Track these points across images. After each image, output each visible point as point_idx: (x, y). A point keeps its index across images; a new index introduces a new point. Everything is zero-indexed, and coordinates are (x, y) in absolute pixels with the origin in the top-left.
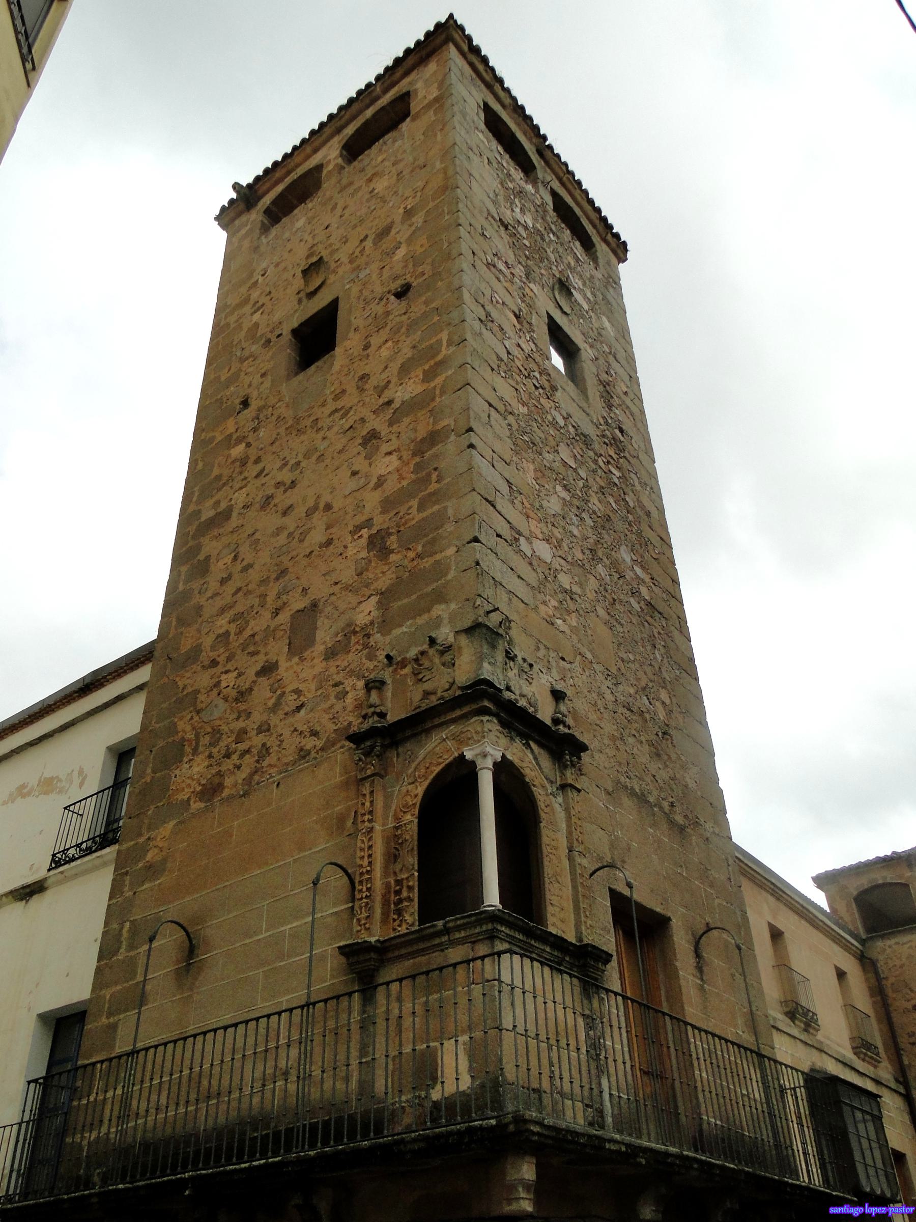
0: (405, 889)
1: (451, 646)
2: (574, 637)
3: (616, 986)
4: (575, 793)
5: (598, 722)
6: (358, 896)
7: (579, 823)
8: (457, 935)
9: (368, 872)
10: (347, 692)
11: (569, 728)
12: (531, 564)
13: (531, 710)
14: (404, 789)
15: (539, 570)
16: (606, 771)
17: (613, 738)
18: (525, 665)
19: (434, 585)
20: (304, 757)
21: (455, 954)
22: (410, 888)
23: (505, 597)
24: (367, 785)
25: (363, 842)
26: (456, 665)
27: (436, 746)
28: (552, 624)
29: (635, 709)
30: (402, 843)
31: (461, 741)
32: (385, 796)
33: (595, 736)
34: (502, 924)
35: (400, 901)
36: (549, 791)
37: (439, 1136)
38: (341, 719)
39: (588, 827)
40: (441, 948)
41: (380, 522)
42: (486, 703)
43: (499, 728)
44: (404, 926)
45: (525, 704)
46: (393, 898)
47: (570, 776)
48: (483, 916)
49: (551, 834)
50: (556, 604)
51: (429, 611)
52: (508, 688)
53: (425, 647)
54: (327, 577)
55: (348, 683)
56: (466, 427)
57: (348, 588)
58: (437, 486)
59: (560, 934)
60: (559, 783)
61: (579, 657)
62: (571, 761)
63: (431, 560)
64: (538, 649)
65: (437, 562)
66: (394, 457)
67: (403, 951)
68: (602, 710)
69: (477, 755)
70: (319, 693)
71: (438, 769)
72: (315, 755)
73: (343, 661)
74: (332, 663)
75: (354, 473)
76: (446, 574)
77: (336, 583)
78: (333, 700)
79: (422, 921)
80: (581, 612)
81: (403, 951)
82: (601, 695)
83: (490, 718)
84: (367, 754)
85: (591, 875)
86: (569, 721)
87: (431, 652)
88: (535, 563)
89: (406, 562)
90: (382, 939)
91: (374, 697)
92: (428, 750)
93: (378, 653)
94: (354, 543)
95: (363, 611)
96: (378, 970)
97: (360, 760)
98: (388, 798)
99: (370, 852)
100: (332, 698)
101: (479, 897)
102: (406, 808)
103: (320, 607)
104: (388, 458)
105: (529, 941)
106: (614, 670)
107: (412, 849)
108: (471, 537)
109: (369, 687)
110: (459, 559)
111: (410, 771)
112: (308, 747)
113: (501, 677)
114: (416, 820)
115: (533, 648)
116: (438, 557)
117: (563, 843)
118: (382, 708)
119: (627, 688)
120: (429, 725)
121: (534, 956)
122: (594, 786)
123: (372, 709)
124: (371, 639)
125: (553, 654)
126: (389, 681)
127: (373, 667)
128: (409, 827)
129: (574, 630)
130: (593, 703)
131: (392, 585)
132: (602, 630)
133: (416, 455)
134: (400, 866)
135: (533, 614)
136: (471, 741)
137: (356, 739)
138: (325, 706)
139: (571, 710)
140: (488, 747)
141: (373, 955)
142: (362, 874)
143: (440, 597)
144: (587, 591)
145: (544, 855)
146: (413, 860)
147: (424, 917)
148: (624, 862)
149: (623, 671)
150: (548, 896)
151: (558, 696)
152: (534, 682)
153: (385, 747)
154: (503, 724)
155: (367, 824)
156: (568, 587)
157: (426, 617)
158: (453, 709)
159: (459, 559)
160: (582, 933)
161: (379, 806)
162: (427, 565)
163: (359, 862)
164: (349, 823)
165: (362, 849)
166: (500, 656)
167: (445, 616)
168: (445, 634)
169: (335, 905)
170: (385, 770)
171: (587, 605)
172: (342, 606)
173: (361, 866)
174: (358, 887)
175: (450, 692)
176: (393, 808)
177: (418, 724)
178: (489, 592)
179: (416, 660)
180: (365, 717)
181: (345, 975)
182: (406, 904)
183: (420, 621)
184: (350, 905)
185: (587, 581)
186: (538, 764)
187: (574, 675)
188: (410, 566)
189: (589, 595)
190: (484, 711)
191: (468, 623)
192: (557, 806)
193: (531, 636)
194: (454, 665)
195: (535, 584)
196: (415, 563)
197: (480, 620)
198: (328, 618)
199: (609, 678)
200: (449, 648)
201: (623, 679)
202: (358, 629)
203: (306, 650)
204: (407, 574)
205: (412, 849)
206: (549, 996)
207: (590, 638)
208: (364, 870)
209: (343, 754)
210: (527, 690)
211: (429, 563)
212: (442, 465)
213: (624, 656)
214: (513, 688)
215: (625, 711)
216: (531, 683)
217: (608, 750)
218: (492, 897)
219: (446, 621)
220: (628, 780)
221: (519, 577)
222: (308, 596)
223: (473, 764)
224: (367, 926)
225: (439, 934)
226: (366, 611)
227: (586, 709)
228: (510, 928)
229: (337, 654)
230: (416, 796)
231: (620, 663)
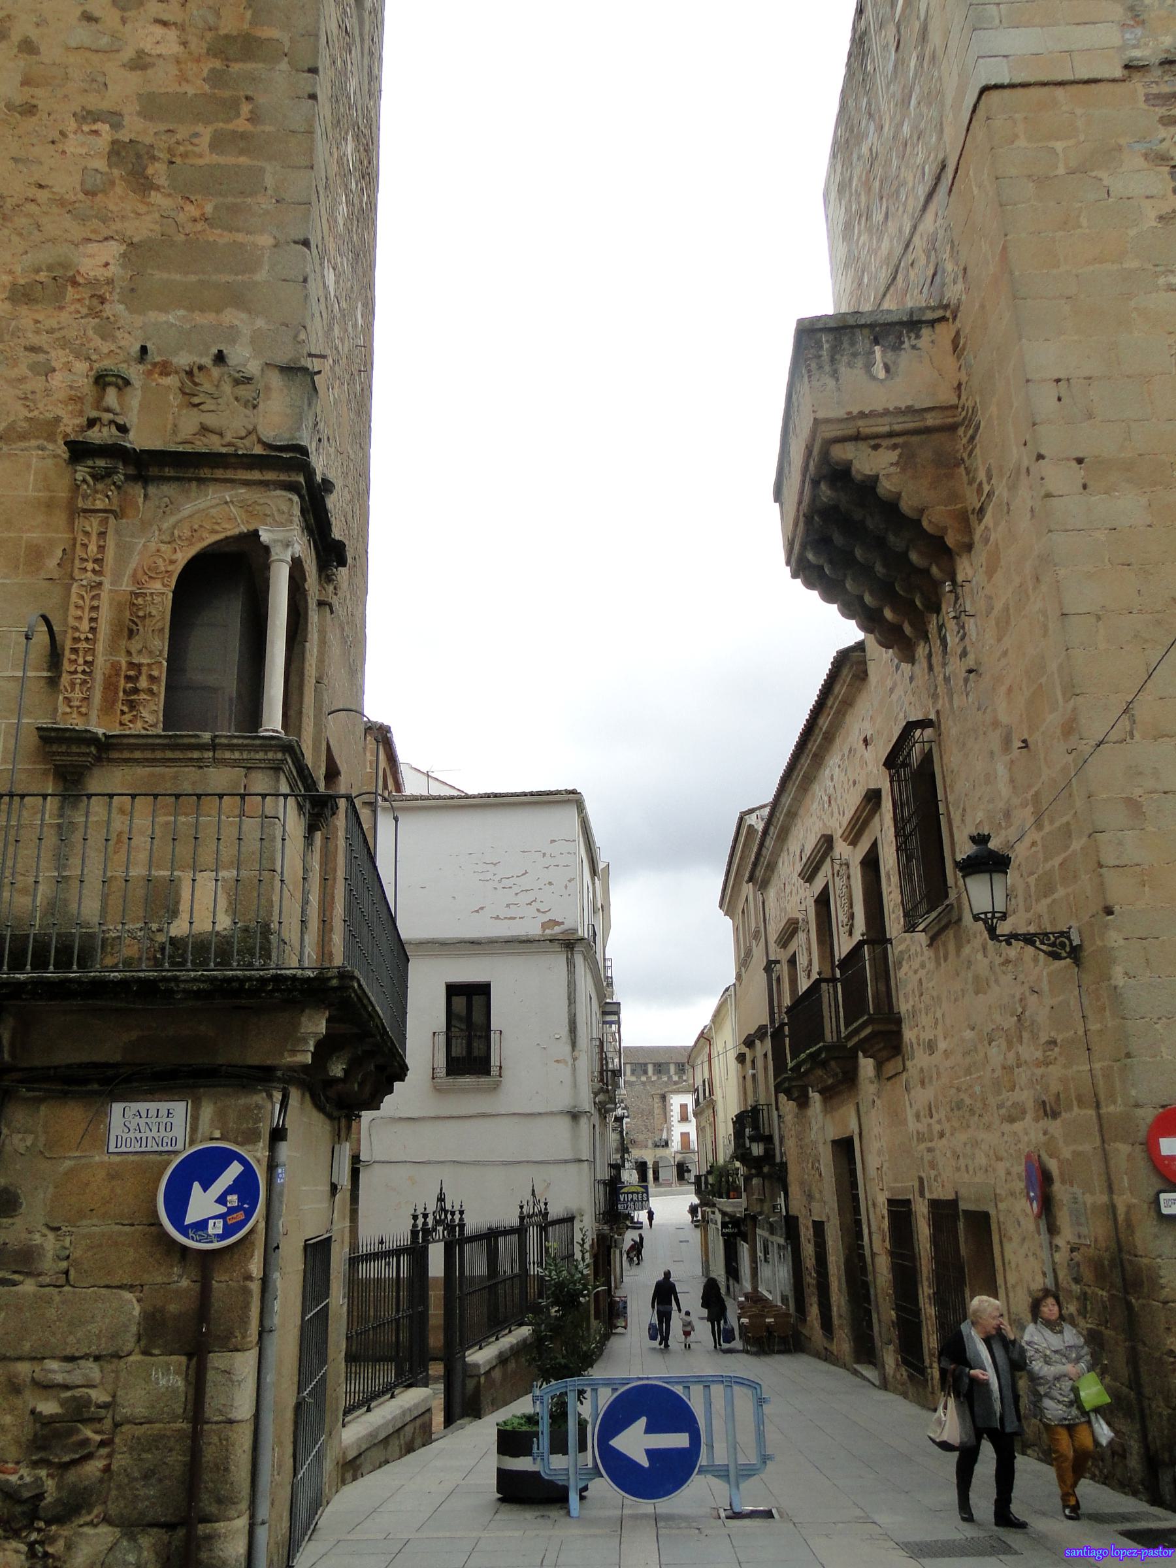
10: (54, 370)
14: (153, 546)
19: (230, 278)
21: (220, 778)
22: (152, 679)
26: (261, 406)
27: (212, 507)
30: (145, 617)
35: (136, 691)
37: (230, 980)
41: (135, 127)
44: (139, 724)
48: (273, 742)
51: (218, 311)
53: (207, 361)
55: (58, 357)
56: (311, 65)
58: (249, 127)
66: (172, 34)
69: (275, 541)
75: (88, 18)
81: (138, 755)
89: (181, 218)
94: (80, 137)
97: (84, 481)
98: (124, 550)
104: (159, 31)
107: (163, 629)
108: (302, 237)
109: (101, 380)
111: (165, 526)
116: (240, 237)
127: (115, 352)
133: (215, 56)
134: (139, 647)
136: (269, 520)
142: (76, 640)
143: (237, 298)
155: (89, 574)
164: (52, 563)
167: (246, 331)
168: (242, 356)
169: (38, 670)
173: (76, 629)
183: (200, 318)
190: (291, 487)
194: (255, 407)
212: (262, 99)
225: (201, 747)
229: (36, 301)
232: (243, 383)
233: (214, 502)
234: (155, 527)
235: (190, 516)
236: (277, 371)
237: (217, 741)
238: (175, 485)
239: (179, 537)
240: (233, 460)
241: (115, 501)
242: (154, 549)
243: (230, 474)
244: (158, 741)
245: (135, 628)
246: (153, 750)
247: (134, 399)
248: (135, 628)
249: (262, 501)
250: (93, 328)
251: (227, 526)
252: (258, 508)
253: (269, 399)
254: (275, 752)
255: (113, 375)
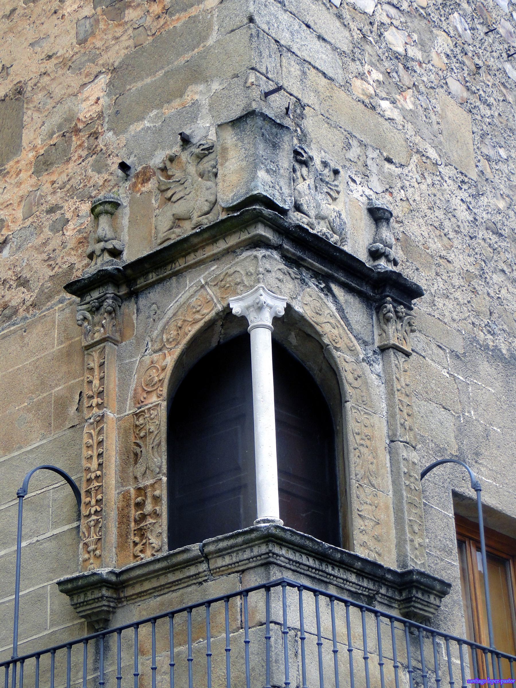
0: (149, 500)
1: (211, 147)
2: (409, 126)
3: (459, 628)
4: (402, 358)
5: (444, 253)
6: (84, 512)
7: (406, 400)
8: (219, 562)
9: (97, 477)
10: (68, 221)
11: (396, 263)
12: (339, 17)
13: (334, 239)
14: (147, 359)
15: (352, 26)
16: (455, 325)
17: (467, 276)
18: (326, 171)
19: (187, 56)
20: (10, 318)
21: (217, 588)
22: (156, 499)
23: (295, 69)
24: (96, 355)
25: (91, 436)
26: (220, 173)
27: (192, 296)
28: (373, 108)
29: (506, 232)
30: (145, 436)
31: (227, 288)
32: (120, 371)
33: (437, 274)
34: (281, 546)
35: (144, 517)
36: (361, 356)
38: (59, 260)
39: (421, 407)
40: (198, 580)
42: (262, 231)
43: (282, 266)
44: (149, 552)
45: (325, 230)
46: (134, 513)
47: (394, 334)
48: (253, 536)
49: (363, 417)
50: (381, 77)
51: (181, 96)
52: (298, 208)
53: (176, 149)
54: (38, 49)
55: (69, 207)
57: (66, 64)
59: (372, 557)
60: (377, 344)
61: (415, 158)
62: (396, 312)
63: (184, 17)
64: (348, 147)
65: (193, 19)
67: (147, 586)
68: (452, 235)
69: (248, 308)
70: (28, 223)
71: (192, 330)
72: (24, 314)
73: (60, 174)
74: (45, 178)
76: (205, 38)
77: (50, 57)
78: (47, 232)
79: (173, 543)
80: (422, 88)
81: (147, 586)
82: (451, 213)
83: (268, 253)
84: (95, 310)
85: (423, 475)
86: (397, 253)
87: (185, 156)
88: (346, 14)
90: (117, 570)
91: (104, 226)
92: (182, 300)
93: (109, 162)
95: (87, 99)
96: (114, 613)
97: (85, 319)
98: (125, 372)
99: (100, 450)
100: (46, 230)
101: (252, 510)
102: (150, 386)
103: (28, 94)
105: (324, 567)
106: (473, 174)
107: (159, 444)
110: (225, 13)
111: (155, 333)
112: (13, 303)
113: (286, 191)
114: (165, 403)
115: (340, 145)
116: (193, 11)
117: (381, 429)
118: (114, 242)
119: (493, 201)
120: (180, 264)
121: (332, 591)
122: (434, 347)
123: (102, 244)
124: (100, 140)
125: (372, 154)
126: (125, 202)
127: (103, 181)
128: (154, 413)
129: (409, 116)
130: (437, 224)
131: (127, 56)
132: (456, 115)
134: (143, 469)
135: (342, 94)
136: (240, 287)
137: (79, 288)
138: (38, 241)
139: (401, 236)
140: (265, 294)
141: (105, 592)
142: (89, 481)
143: (196, 74)
144: (433, 55)
145: (351, 448)
146: (159, 459)
147: (178, 536)
148: (477, 454)
149: (488, 174)
150: (355, 505)
151: (378, 216)
152: (342, 197)
153: (119, 299)
154: (291, 261)
155: (95, 410)
156: (400, 50)
157: (176, 103)
158: (214, 240)
159: (225, 13)
160: (406, 556)
161: (112, 386)
162: (178, 25)
163: (85, 464)
165: (89, 447)
166: (285, 160)
167: (205, 101)
168: (203, 129)
170: (122, 335)
171: (433, 77)
172: (58, 91)
173: (88, 470)
174: (84, 499)
175: (210, 216)
176: (133, 386)
177: (163, 263)
178: (268, 63)
179: (164, 170)
180: (91, 256)
181: (73, 619)
182: (152, 521)
183: (169, 110)
184: (75, 524)
185: (433, 38)
186: (344, 318)
187: (407, 184)
188: (156, 26)
189: (436, 60)
191: (236, 112)
192: (374, 377)
193: (338, 127)
194: (216, 175)
195: (345, 47)
196: (162, 21)
197: (254, 106)
198: (38, 110)
199: (465, 187)
200: (210, 149)
201: (488, 188)
202: (81, 126)
203: (8, 160)
204: (150, 38)
205: (159, 444)
206: (358, 643)
207: (436, 127)
208: (93, 476)
209: (64, 309)
210: (329, 208)
211: (183, 20)
213: (491, 153)
214: (305, 208)
215: (489, 235)
216: (334, 199)
217: (458, 294)
218: (269, 507)
219: (205, 111)
220: (489, 336)
221: (320, 38)
222: (10, 78)
223: (243, 320)
224: (98, 552)
226: (93, 98)
227: (426, 234)
228: (295, 551)
230: (163, 369)
231: (484, 163)
232: (206, 156)
233: (192, 291)
234: (148, 339)
235: (174, 315)
236: (230, 128)
237: (206, 550)
238: (158, 288)
239: (168, 340)
240: (195, 240)
241: (109, 328)
242: (148, 362)
243: (200, 255)
244: (158, 566)
245: (138, 450)
246: (158, 577)
247: (125, 217)
248: (138, 450)
249: (231, 271)
250: (92, 165)
251: (205, 311)
252: (229, 279)
253: (227, 160)
254: (259, 545)
255: (101, 204)
